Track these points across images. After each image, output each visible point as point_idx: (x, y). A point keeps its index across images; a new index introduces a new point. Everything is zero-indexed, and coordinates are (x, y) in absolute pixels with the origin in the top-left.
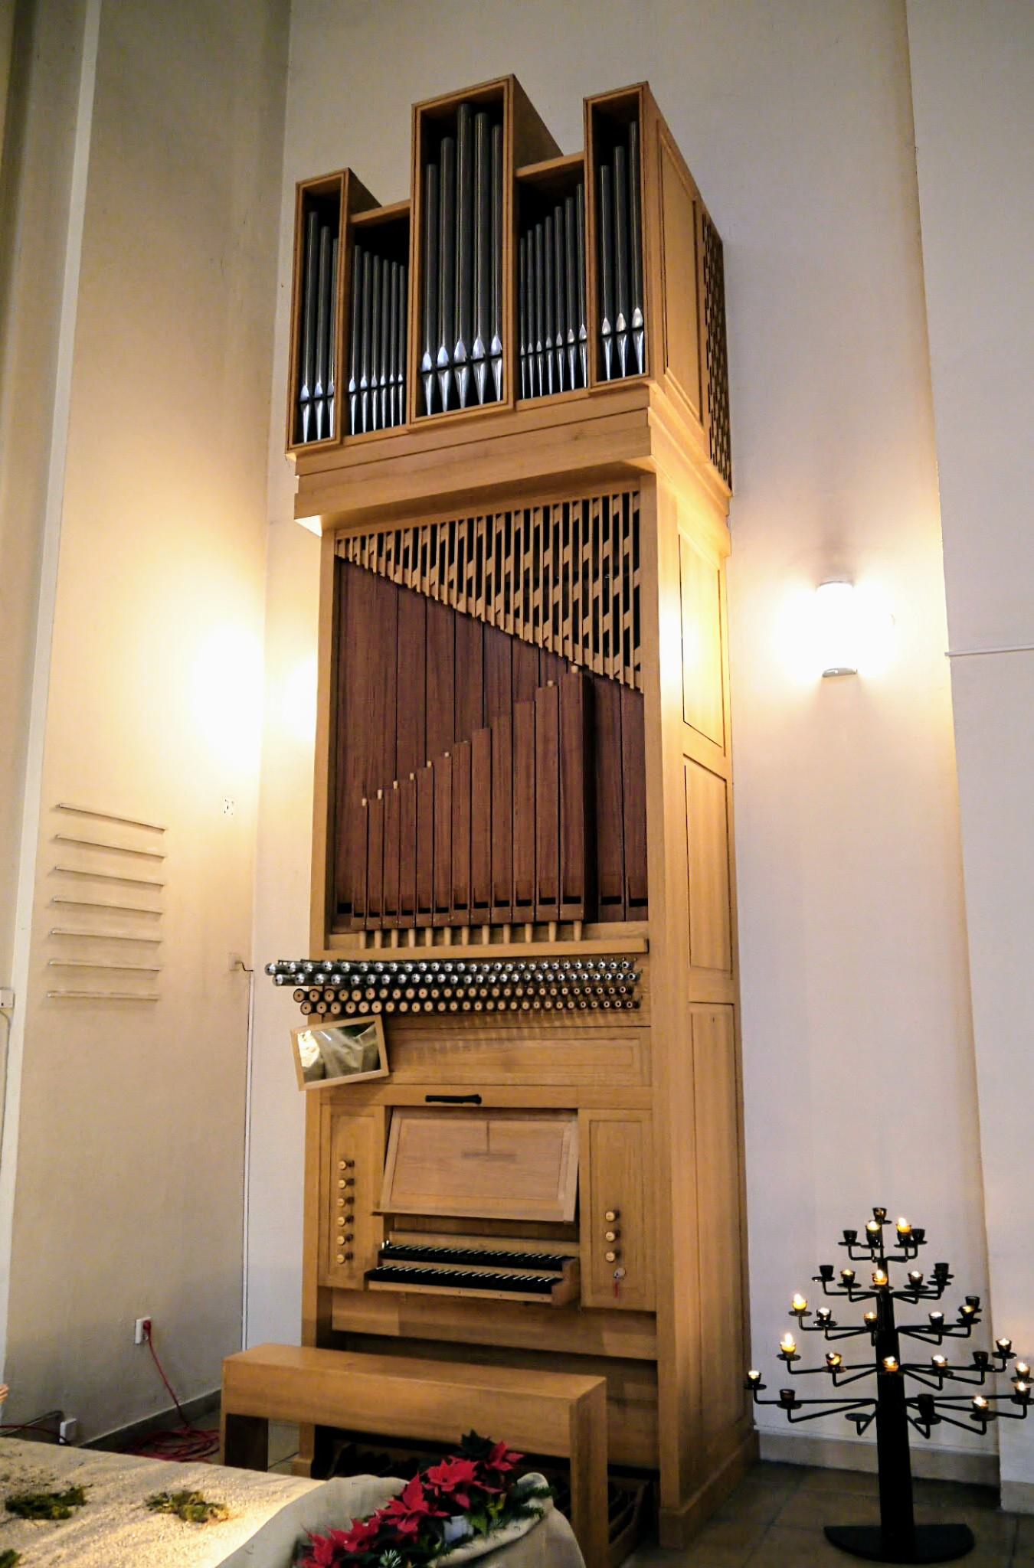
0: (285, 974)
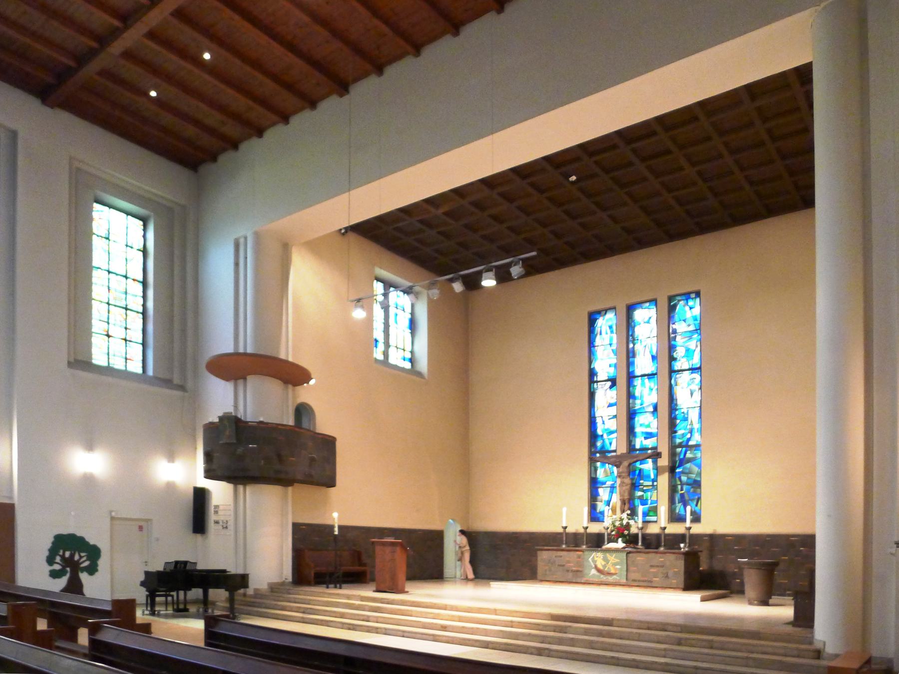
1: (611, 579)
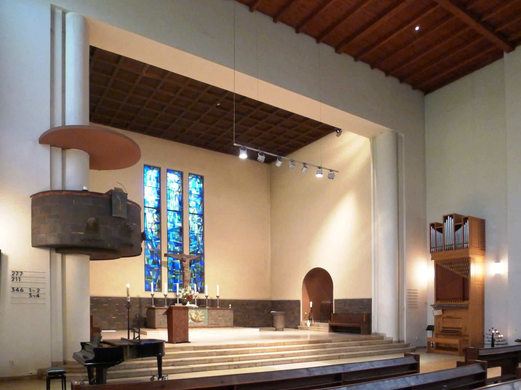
0: (432, 305)
1: (199, 324)
